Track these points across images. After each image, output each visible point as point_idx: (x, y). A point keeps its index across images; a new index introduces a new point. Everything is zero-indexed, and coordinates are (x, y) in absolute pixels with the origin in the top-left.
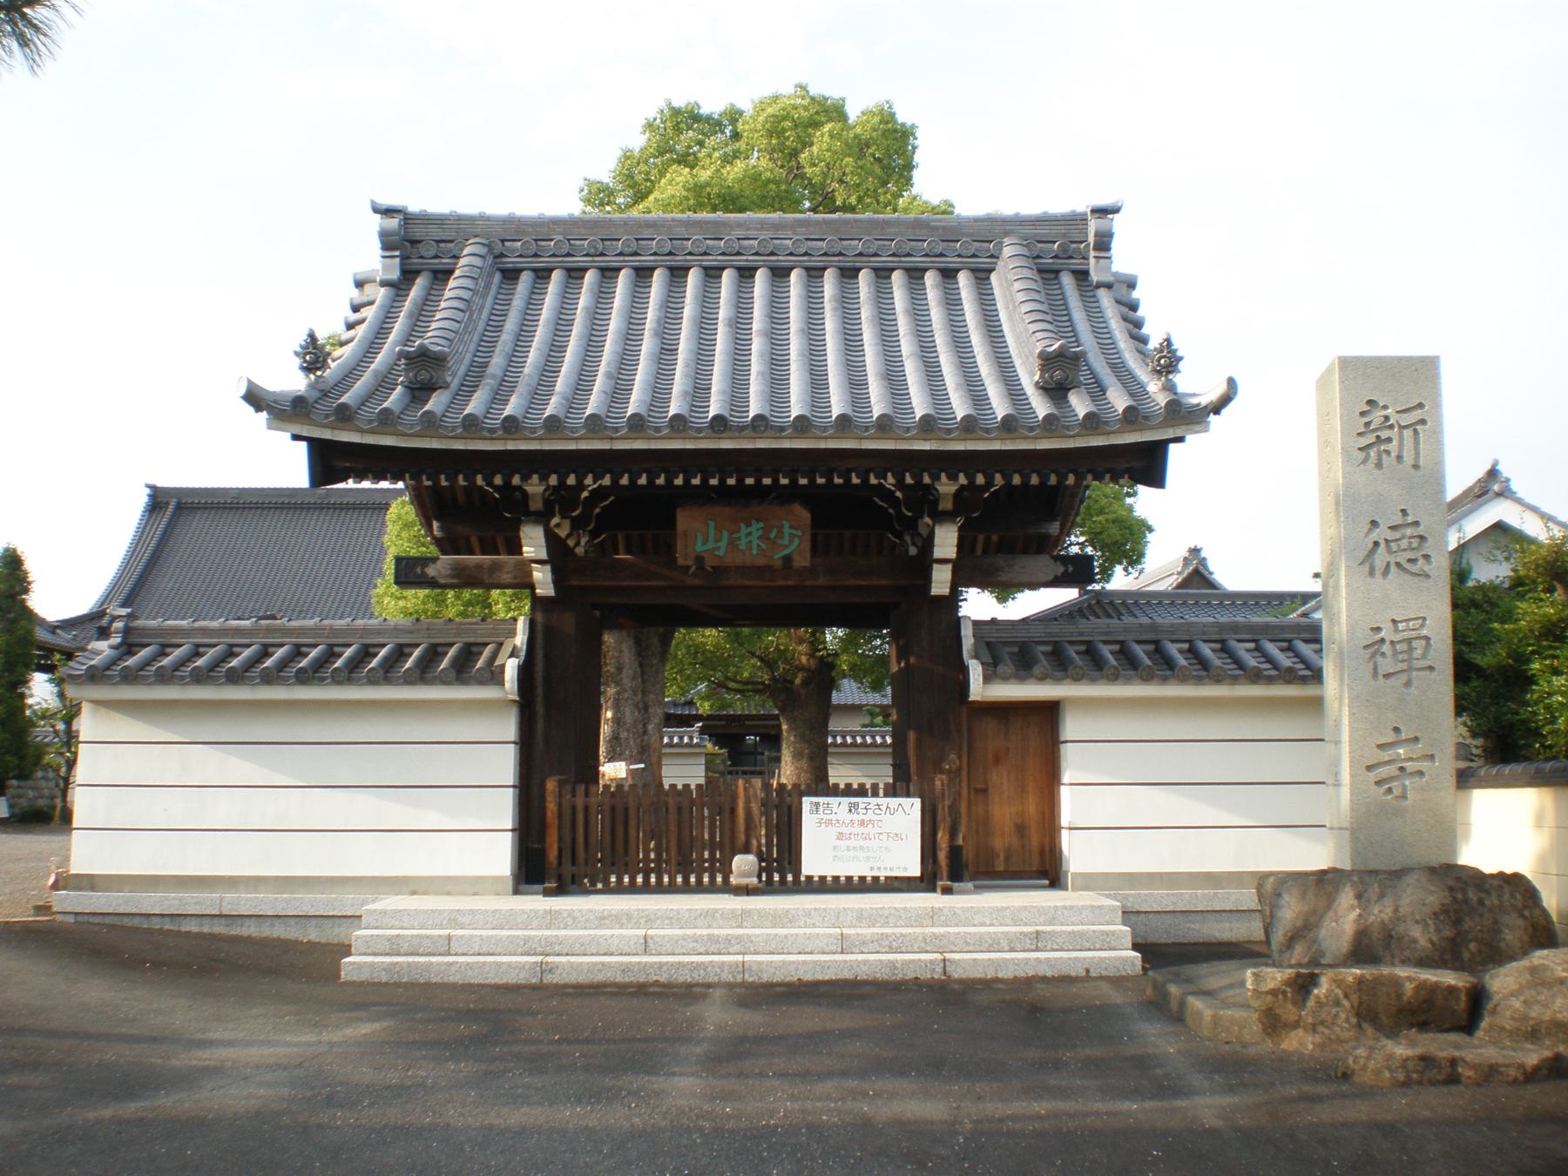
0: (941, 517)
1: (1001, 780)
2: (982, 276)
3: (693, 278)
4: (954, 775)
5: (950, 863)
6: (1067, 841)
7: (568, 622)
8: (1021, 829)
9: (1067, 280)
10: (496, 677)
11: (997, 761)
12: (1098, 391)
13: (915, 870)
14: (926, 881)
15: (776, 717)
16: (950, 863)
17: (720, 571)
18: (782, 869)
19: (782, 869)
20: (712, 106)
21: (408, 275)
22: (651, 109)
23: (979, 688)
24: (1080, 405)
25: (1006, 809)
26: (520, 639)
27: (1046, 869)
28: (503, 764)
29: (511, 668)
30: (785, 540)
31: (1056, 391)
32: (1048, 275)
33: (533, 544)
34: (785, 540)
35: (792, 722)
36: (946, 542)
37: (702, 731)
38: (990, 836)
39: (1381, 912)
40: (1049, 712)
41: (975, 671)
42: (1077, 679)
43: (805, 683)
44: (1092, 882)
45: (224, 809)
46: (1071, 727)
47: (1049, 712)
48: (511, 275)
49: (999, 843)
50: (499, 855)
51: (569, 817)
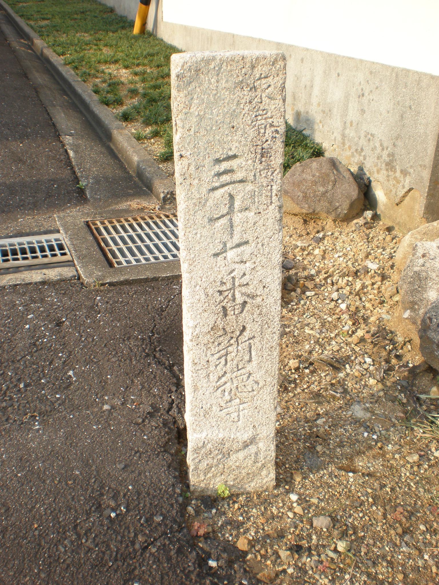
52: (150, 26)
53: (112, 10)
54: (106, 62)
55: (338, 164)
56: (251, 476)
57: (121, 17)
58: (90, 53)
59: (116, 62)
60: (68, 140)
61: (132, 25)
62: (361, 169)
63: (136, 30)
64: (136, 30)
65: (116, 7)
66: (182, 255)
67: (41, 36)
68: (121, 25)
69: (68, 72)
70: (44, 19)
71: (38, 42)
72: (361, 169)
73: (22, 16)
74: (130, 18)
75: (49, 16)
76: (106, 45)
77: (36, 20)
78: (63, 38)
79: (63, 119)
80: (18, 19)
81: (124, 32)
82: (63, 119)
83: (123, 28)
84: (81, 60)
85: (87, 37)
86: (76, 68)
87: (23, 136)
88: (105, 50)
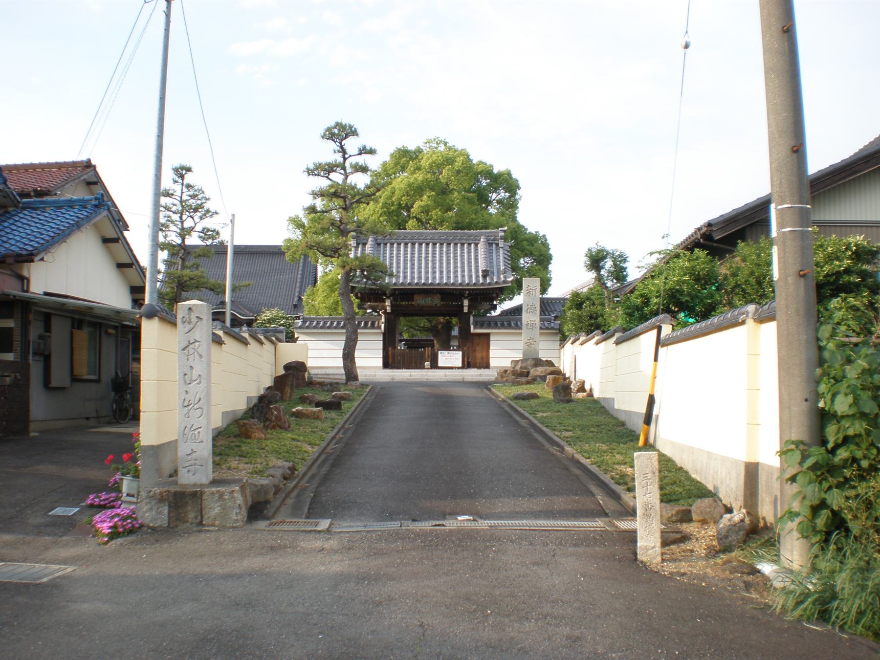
0: (466, 298)
1: (478, 348)
2: (476, 245)
3: (417, 245)
4: (468, 348)
5: (467, 364)
6: (491, 361)
7: (392, 317)
8: (482, 358)
9: (494, 246)
10: (379, 328)
11: (478, 344)
12: (492, 278)
13: (460, 365)
14: (463, 367)
15: (432, 341)
16: (467, 364)
17: (423, 307)
18: (434, 365)
19: (434, 365)
20: (412, 147)
21: (358, 244)
22: (392, 150)
23: (472, 330)
24: (488, 280)
25: (479, 355)
26: (383, 320)
27: (487, 366)
28: (380, 345)
29: (383, 326)
30: (436, 301)
31: (485, 277)
32: (490, 244)
33: (388, 303)
34: (436, 301)
35: (438, 340)
36: (466, 303)
37: (405, 345)
38: (476, 358)
39: (524, 365)
40: (488, 335)
41: (472, 327)
42: (492, 329)
43: (442, 327)
44: (495, 368)
45: (325, 353)
46: (492, 338)
47: (488, 335)
48: (379, 244)
49: (478, 361)
50: (379, 362)
51: (394, 355)
52: (651, 440)
53: (623, 424)
54: (618, 464)
55: (99, 510)
56: (655, 558)
57: (631, 431)
58: (607, 458)
59: (625, 464)
60: (599, 497)
61: (638, 439)
62: (161, 500)
63: (641, 443)
64: (641, 443)
65: (627, 422)
66: (636, 483)
67: (570, 445)
68: (630, 438)
69: (594, 469)
70: (567, 430)
71: (568, 449)
72: (161, 500)
73: (547, 426)
74: (638, 433)
75: (571, 428)
76: (618, 453)
77: (560, 431)
78: (587, 447)
79: (594, 489)
80: (545, 429)
81: (632, 444)
82: (594, 489)
83: (632, 441)
84: (602, 461)
85: (604, 447)
86: (599, 466)
87: (576, 495)
88: (617, 456)
